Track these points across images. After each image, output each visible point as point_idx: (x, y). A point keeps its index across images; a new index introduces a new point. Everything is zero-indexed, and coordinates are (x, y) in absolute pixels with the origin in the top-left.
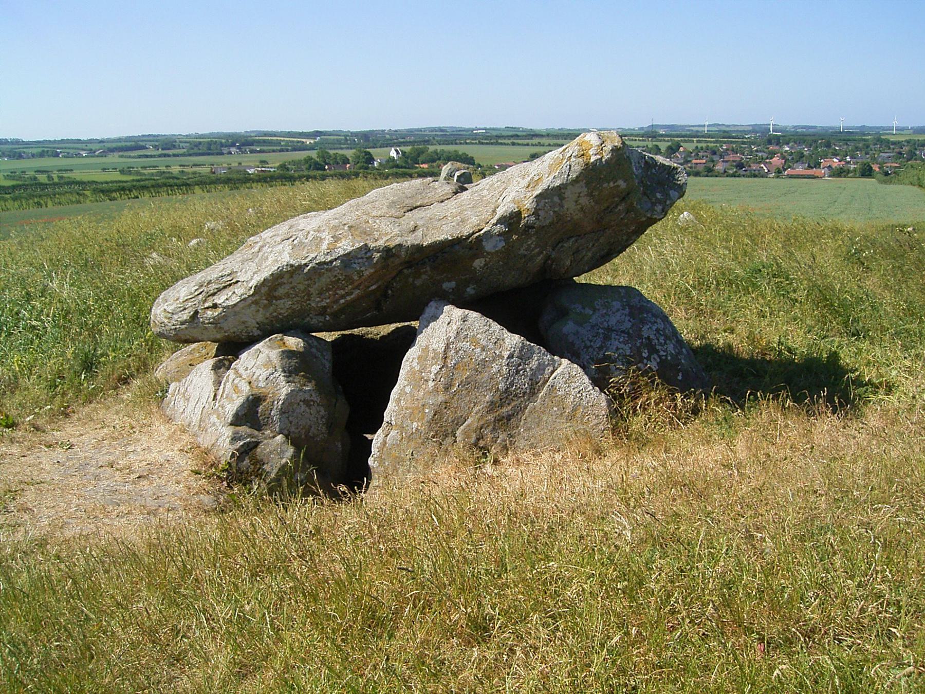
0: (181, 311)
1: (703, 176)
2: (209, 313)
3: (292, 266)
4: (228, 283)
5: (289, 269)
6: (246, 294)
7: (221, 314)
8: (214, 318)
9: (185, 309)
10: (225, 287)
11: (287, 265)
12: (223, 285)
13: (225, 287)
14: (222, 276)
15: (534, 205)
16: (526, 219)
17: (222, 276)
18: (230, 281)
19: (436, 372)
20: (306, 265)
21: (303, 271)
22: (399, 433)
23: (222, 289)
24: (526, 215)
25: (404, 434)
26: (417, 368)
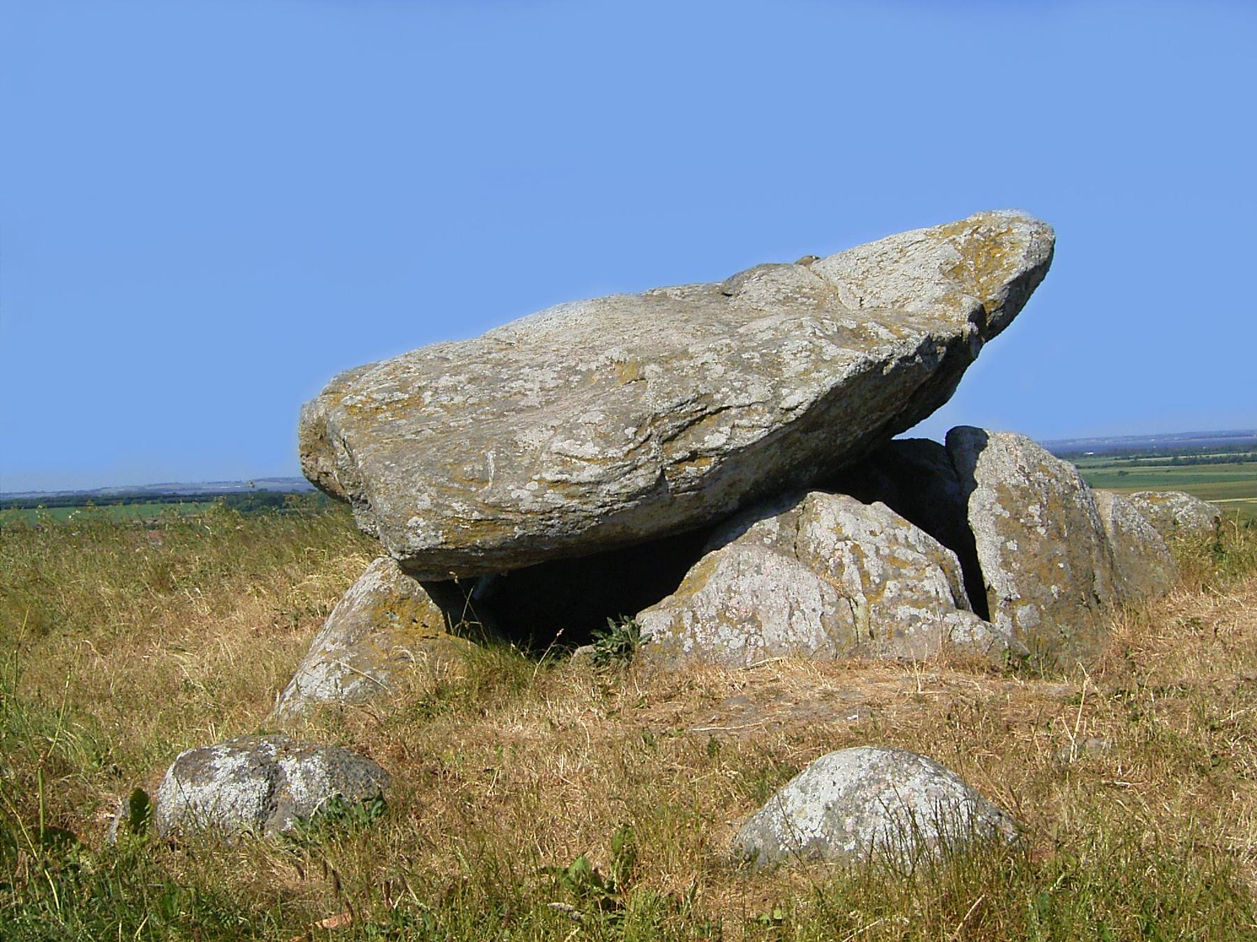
0: (625, 474)
1: (219, 495)
2: (690, 469)
3: (871, 363)
4: (699, 414)
5: (868, 369)
6: (780, 422)
7: (715, 467)
8: (701, 478)
9: (635, 468)
10: (692, 423)
11: (865, 363)
12: (689, 419)
13: (692, 423)
14: (682, 405)
15: (1005, 294)
16: (993, 315)
17: (682, 405)
18: (702, 410)
19: (1038, 513)
20: (886, 363)
21: (882, 371)
22: (1035, 608)
23: (687, 426)
24: (993, 310)
25: (1042, 607)
26: (1007, 514)
